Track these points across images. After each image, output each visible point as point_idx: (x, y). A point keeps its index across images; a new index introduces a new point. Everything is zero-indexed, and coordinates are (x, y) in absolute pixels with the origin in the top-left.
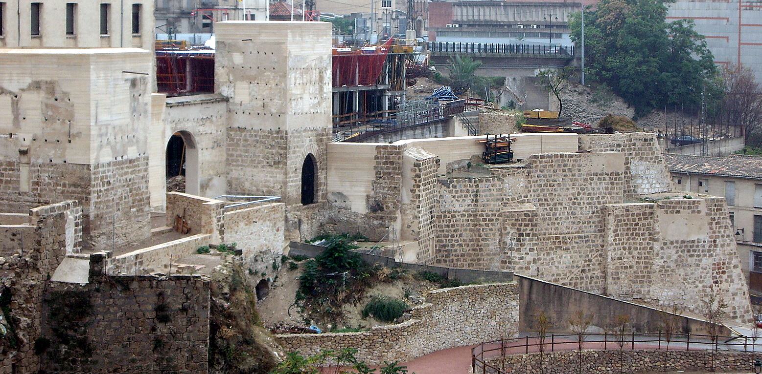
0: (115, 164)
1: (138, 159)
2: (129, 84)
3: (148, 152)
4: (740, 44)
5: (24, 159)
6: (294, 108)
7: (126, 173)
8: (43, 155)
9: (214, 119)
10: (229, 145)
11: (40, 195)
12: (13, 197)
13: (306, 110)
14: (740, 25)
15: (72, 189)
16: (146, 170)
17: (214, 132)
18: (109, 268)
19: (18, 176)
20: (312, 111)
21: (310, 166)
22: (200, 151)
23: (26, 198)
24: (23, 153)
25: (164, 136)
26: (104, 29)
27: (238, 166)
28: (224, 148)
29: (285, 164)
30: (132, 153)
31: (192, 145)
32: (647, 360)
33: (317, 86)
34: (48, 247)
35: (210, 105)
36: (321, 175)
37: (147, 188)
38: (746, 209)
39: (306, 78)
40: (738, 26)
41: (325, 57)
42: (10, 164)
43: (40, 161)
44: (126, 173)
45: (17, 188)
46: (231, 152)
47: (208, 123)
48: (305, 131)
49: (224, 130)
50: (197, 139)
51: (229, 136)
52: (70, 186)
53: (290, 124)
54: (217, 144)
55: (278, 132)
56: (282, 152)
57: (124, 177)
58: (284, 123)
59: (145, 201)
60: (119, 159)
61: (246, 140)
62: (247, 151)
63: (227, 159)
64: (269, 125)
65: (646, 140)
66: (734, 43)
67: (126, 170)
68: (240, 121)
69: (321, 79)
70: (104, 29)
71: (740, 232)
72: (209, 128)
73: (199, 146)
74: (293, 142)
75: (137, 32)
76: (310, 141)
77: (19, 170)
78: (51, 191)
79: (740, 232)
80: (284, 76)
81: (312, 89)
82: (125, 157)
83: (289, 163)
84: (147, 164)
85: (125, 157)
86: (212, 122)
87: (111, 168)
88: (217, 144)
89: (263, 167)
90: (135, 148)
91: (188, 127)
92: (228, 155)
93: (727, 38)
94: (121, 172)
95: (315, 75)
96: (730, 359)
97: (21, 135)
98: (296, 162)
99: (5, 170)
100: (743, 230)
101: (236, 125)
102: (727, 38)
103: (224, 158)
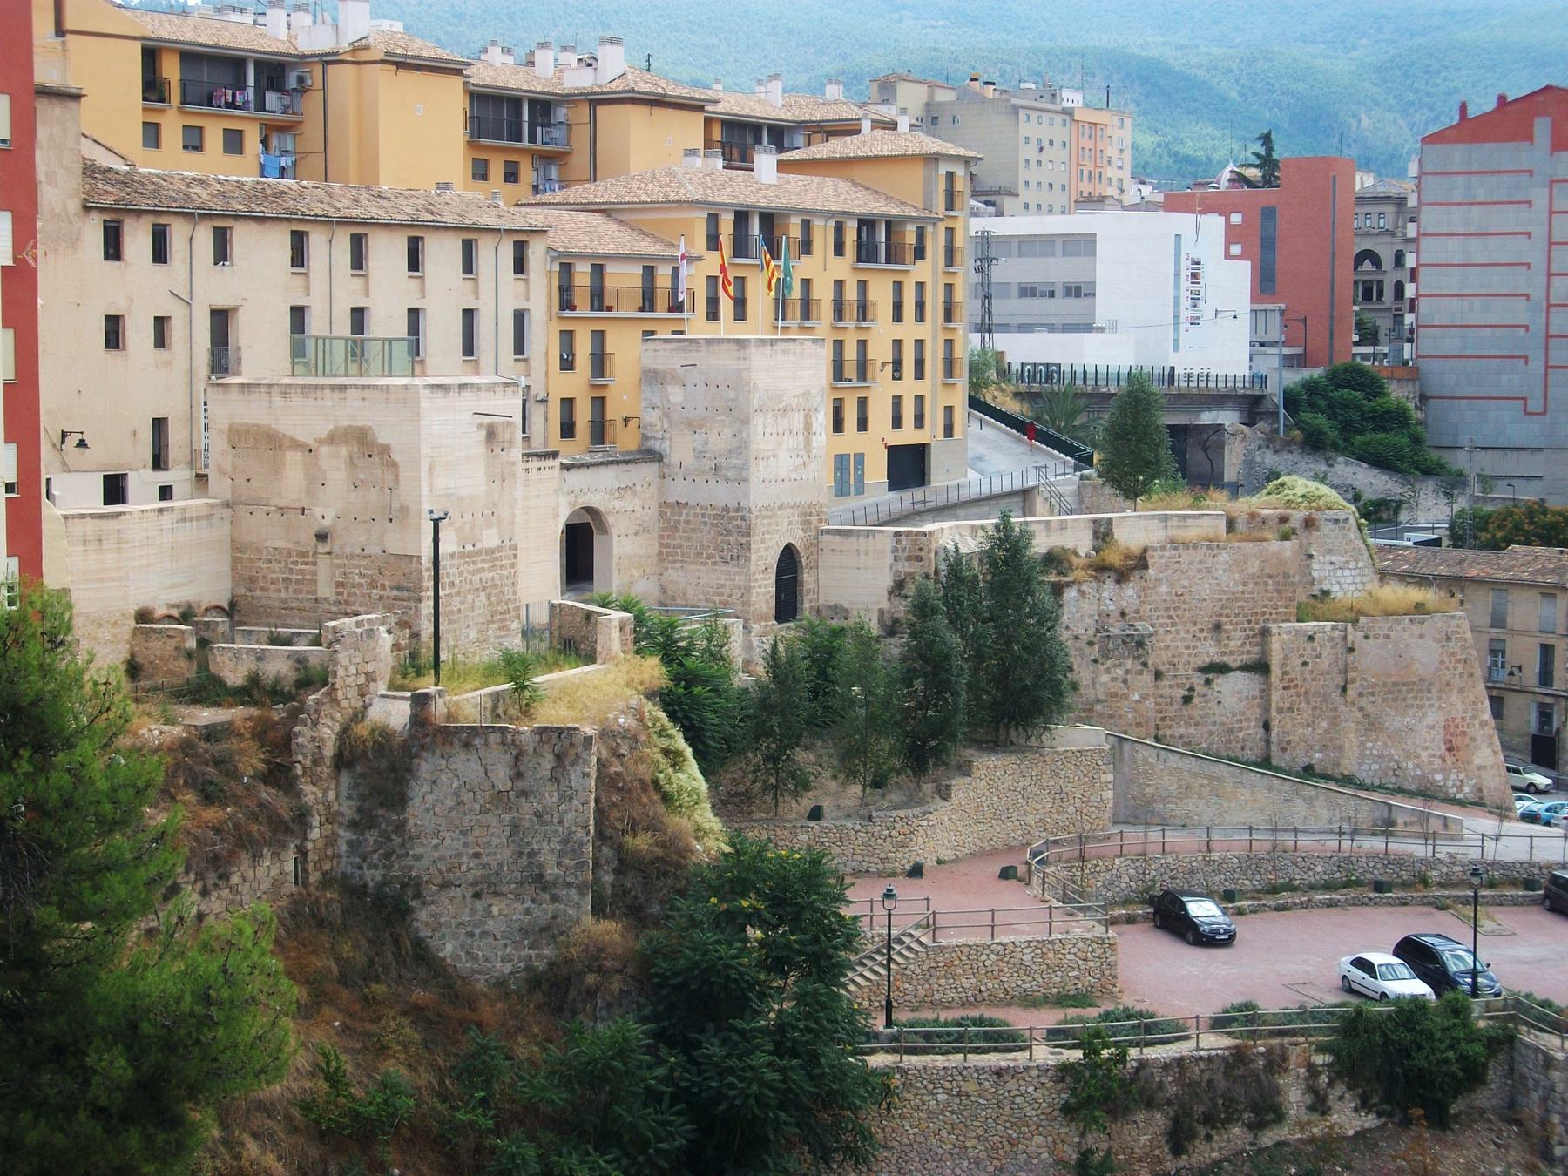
0: (462, 555)
1: (499, 549)
2: (484, 433)
3: (517, 539)
4: (1547, 367)
5: (322, 548)
6: (758, 472)
7: (481, 570)
8: (352, 539)
9: (638, 488)
10: (663, 530)
11: (347, 603)
12: (308, 605)
13: (783, 473)
14: (1548, 336)
15: (395, 593)
16: (513, 565)
17: (638, 509)
18: (439, 709)
19: (315, 573)
20: (793, 476)
21: (789, 562)
22: (615, 538)
23: (327, 606)
24: (322, 537)
25: (556, 516)
26: (469, 348)
27: (674, 562)
28: (656, 535)
29: (748, 559)
30: (490, 539)
31: (604, 530)
32: (1319, 869)
33: (801, 438)
34: (349, 681)
35: (631, 467)
36: (807, 578)
37: (515, 592)
38: (1525, 633)
39: (784, 424)
40: (1543, 340)
41: (814, 392)
42: (303, 554)
43: (348, 551)
44: (481, 570)
45: (314, 592)
46: (666, 541)
47: (628, 496)
48: (781, 507)
49: (655, 506)
50: (610, 520)
51: (662, 514)
52: (392, 588)
53: (758, 496)
54: (642, 529)
55: (737, 510)
56: (743, 540)
57: (477, 577)
58: (746, 495)
59: (513, 613)
60: (469, 547)
61: (688, 522)
62: (689, 539)
63: (660, 553)
64: (721, 495)
65: (1337, 521)
66: (1536, 366)
67: (480, 565)
68: (679, 491)
69: (808, 427)
70: (469, 348)
71: (1516, 671)
72: (628, 503)
73: (614, 531)
74: (760, 525)
75: (418, 354)
76: (790, 523)
77: (315, 564)
78: (363, 595)
79: (1516, 671)
80: (745, 421)
81: (797, 441)
82: (479, 546)
83: (753, 557)
84: (515, 556)
85: (479, 546)
86: (634, 493)
87: (456, 562)
88: (642, 529)
89: (714, 564)
90: (494, 530)
91: (595, 501)
92: (661, 545)
93: (1526, 358)
94: (471, 567)
95: (798, 420)
96: (1457, 869)
97: (318, 511)
98: (765, 555)
99: (295, 563)
100: (1520, 668)
101: (672, 500)
102: (1526, 358)
103: (656, 548)
